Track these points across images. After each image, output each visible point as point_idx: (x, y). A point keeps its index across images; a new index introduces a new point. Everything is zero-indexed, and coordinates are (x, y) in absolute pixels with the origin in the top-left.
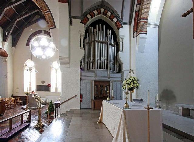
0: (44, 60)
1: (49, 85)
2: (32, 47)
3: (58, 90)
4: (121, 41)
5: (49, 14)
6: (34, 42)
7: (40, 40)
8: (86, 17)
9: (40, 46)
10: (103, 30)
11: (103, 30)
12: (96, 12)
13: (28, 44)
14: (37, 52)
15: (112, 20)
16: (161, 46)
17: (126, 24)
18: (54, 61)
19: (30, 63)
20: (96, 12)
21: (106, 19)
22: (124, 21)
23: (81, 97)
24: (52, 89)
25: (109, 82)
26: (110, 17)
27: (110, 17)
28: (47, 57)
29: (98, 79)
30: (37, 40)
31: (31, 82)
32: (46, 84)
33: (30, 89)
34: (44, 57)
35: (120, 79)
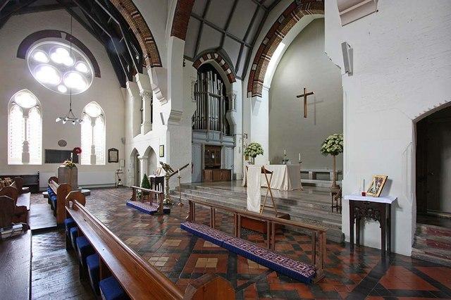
0: (63, 96)
1: (77, 151)
2: (34, 64)
3: (97, 160)
4: (233, 97)
5: (152, 43)
6: (37, 54)
7: (54, 51)
8: (198, 60)
9: (51, 63)
10: (214, 80)
11: (214, 80)
12: (209, 56)
13: (22, 53)
14: (45, 75)
15: (226, 70)
16: (272, 110)
17: (238, 78)
18: (37, 96)
19: (24, 99)
20: (209, 56)
21: (218, 66)
22: (237, 75)
23: (193, 165)
24: (85, 159)
25: (220, 147)
26: (223, 66)
27: (223, 66)
28: (70, 91)
29: (210, 143)
30: (47, 50)
31: (96, 145)
32: (69, 147)
33: (26, 156)
34: (62, 90)
35: (232, 144)
